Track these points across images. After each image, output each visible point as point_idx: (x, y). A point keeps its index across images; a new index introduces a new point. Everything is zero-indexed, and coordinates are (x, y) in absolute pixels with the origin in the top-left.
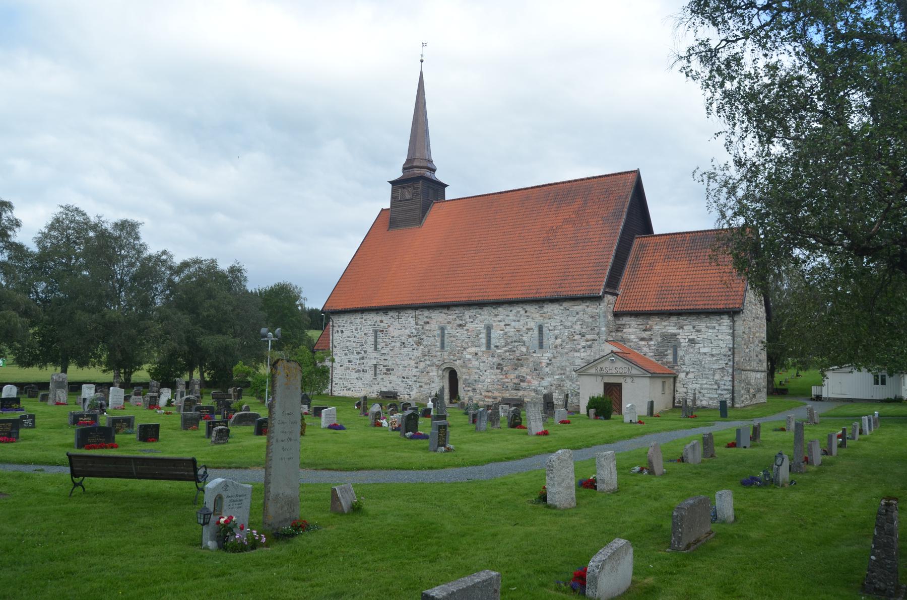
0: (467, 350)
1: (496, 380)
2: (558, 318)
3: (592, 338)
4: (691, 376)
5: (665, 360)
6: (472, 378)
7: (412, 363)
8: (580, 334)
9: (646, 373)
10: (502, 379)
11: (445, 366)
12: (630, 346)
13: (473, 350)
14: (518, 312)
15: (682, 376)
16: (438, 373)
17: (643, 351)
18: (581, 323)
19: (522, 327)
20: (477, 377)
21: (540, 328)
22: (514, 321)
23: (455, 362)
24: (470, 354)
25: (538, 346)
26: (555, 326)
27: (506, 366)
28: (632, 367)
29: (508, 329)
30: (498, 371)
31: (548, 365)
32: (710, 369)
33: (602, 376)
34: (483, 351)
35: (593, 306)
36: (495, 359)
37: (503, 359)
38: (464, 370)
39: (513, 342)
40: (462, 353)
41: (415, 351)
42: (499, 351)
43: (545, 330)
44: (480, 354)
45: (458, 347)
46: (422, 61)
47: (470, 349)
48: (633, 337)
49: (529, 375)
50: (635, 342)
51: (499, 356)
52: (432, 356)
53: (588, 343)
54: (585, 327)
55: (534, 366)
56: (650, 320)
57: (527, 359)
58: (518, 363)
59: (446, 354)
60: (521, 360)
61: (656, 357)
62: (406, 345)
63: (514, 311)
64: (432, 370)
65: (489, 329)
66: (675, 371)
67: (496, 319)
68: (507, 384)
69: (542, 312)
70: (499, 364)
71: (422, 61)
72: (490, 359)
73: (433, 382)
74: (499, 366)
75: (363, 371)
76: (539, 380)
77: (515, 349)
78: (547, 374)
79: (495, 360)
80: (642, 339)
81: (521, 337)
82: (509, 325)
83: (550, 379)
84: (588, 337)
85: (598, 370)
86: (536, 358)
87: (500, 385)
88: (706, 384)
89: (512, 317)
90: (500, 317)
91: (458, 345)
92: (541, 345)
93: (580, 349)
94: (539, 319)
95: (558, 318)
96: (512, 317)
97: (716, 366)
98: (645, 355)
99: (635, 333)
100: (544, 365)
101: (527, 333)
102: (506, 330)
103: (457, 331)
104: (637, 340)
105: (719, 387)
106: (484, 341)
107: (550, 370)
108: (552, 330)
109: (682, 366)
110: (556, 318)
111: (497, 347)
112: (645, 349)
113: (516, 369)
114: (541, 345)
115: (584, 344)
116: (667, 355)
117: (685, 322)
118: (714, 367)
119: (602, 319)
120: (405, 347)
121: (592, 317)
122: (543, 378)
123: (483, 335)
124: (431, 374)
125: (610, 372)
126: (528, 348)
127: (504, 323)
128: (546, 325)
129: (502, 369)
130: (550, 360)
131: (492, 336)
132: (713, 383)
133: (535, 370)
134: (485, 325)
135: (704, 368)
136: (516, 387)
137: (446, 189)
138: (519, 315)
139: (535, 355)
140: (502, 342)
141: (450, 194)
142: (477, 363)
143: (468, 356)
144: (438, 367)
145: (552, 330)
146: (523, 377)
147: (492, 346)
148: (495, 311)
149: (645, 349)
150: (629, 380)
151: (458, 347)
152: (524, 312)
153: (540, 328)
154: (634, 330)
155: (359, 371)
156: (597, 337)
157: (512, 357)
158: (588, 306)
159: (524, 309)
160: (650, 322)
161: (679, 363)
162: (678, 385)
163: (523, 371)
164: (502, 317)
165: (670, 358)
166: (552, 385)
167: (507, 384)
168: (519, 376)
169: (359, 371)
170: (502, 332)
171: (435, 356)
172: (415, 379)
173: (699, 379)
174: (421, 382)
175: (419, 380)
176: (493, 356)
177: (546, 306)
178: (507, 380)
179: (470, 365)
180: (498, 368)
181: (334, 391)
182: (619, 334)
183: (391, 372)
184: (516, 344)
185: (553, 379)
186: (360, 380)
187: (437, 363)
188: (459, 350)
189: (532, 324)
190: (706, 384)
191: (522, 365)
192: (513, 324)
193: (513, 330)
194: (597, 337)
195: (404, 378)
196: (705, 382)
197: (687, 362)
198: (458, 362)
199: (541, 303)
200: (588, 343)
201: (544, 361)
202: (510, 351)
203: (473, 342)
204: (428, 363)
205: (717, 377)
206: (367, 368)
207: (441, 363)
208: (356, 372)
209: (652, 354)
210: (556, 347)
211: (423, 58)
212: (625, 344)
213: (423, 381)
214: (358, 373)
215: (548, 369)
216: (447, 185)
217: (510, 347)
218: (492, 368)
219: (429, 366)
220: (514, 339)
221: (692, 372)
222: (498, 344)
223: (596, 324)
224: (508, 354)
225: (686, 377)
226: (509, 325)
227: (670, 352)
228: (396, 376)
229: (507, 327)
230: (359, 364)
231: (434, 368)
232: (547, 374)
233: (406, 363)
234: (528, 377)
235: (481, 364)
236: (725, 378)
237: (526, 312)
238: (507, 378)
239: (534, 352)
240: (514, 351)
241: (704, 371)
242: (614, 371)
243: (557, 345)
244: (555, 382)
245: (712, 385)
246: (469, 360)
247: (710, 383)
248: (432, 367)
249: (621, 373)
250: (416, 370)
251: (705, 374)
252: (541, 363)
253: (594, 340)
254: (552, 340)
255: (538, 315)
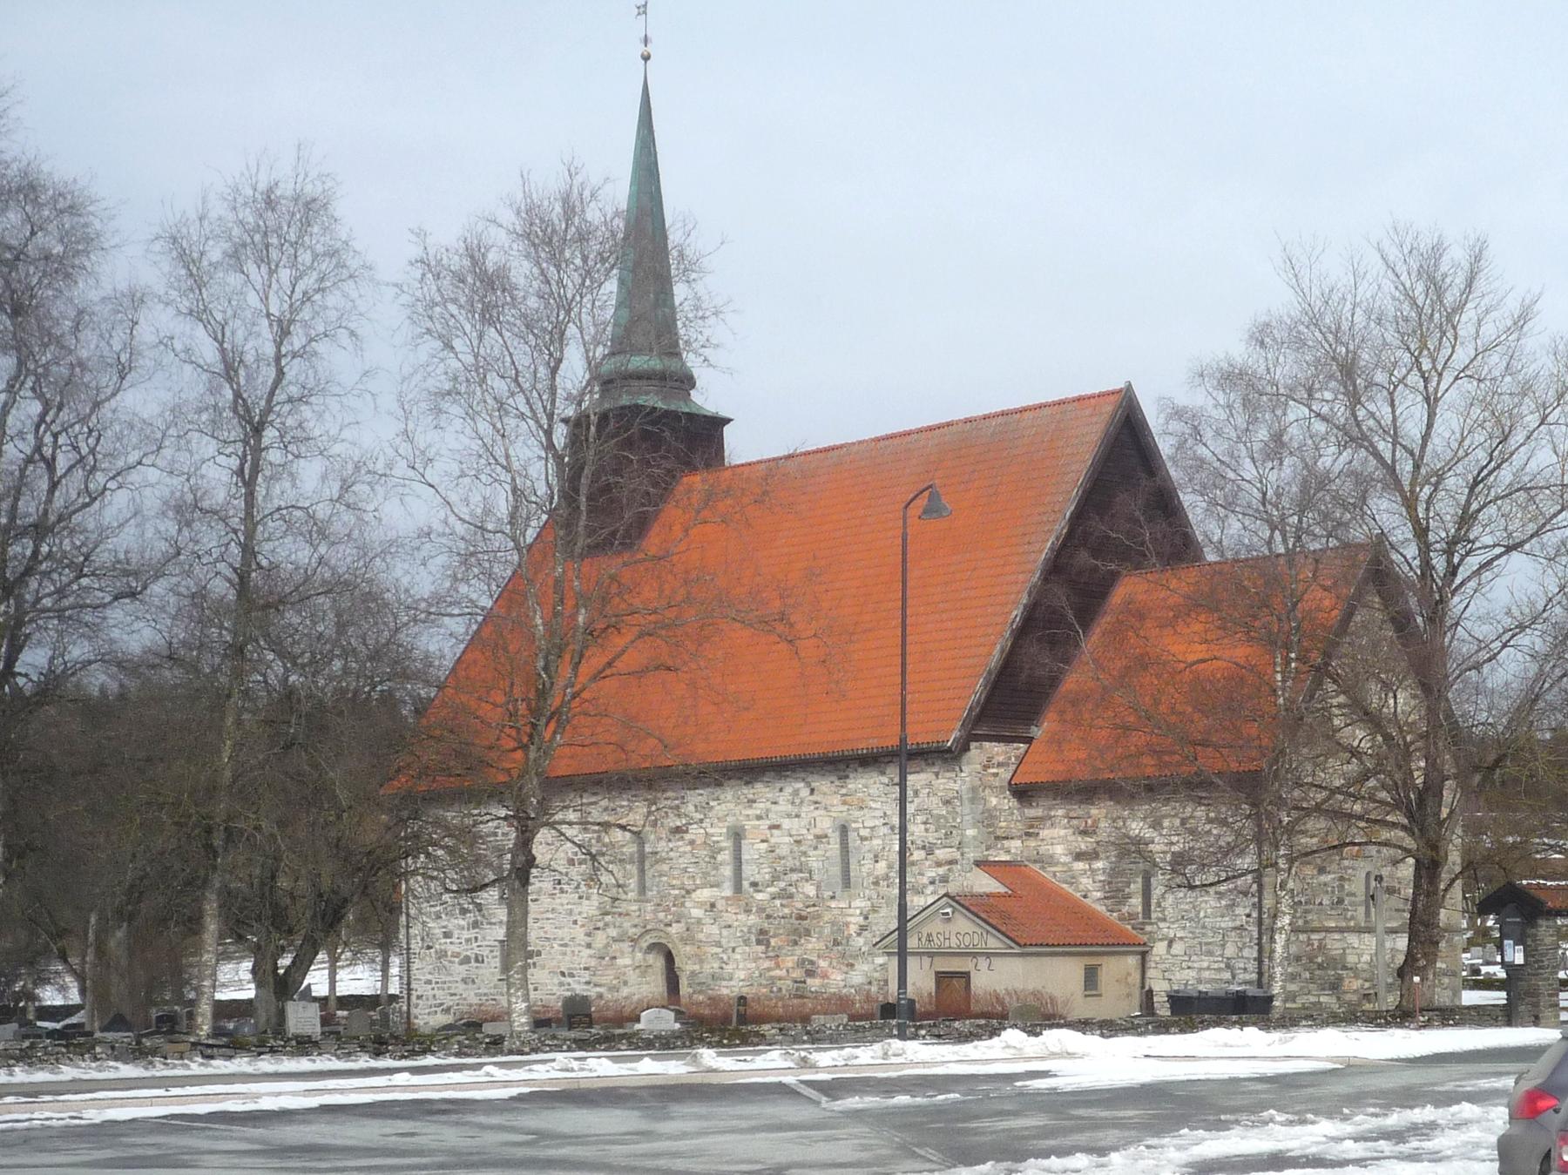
0: (693, 895)
1: (757, 974)
2: (878, 805)
3: (949, 857)
4: (1178, 948)
5: (1125, 909)
6: (707, 968)
7: (579, 933)
8: (924, 848)
9: (1013, 945)
10: (769, 969)
11: (649, 940)
12: (1055, 876)
13: (705, 894)
14: (796, 792)
15: (1160, 948)
16: (633, 958)
17: (1081, 887)
18: (923, 818)
19: (805, 832)
20: (716, 965)
21: (844, 830)
22: (789, 816)
23: (669, 929)
24: (700, 904)
25: (839, 881)
26: (872, 828)
27: (774, 936)
28: (988, 932)
29: (777, 837)
30: (761, 948)
31: (863, 928)
32: (1215, 930)
33: (931, 955)
34: (727, 899)
35: (948, 775)
36: (752, 917)
37: (768, 917)
38: (688, 948)
39: (788, 870)
40: (683, 904)
41: (585, 902)
42: (759, 896)
43: (852, 836)
44: (720, 905)
45: (673, 887)
46: (646, 58)
47: (698, 892)
48: (1059, 850)
49: (824, 958)
50: (1064, 864)
51: (761, 910)
52: (620, 914)
53: (941, 871)
54: (932, 828)
55: (832, 933)
56: (1093, 804)
57: (819, 916)
58: (801, 926)
59: (649, 907)
60: (806, 918)
61: (1108, 902)
62: (565, 887)
63: (788, 790)
64: (622, 953)
65: (737, 835)
66: (1145, 938)
67: (749, 812)
68: (779, 983)
69: (844, 791)
70: (762, 932)
71: (646, 58)
72: (742, 917)
73: (625, 983)
74: (762, 937)
75: (477, 960)
76: (845, 969)
77: (793, 890)
78: (860, 954)
79: (753, 919)
80: (1079, 856)
81: (803, 859)
82: (777, 827)
83: (866, 967)
84: (941, 854)
85: (923, 940)
86: (836, 912)
87: (766, 986)
88: (1208, 968)
89: (784, 806)
90: (759, 808)
91: (674, 882)
92: (847, 882)
93: (925, 887)
94: (839, 810)
95: (878, 805)
96: (784, 806)
97: (1227, 923)
98: (1085, 897)
99: (1064, 840)
100: (853, 929)
101: (816, 848)
102: (773, 840)
103: (671, 845)
104: (1068, 859)
105: (1234, 977)
106: (727, 871)
107: (865, 944)
108: (866, 839)
109: (1162, 925)
110: (874, 805)
111: (754, 884)
112: (1084, 880)
113: (796, 943)
114: (847, 882)
115: (931, 873)
116: (1129, 896)
117: (1165, 810)
118: (1223, 925)
119: (967, 808)
120: (562, 891)
121: (947, 802)
122: (852, 965)
123: (725, 856)
124: (619, 962)
125: (947, 944)
126: (818, 888)
127: (768, 822)
128: (853, 825)
129: (768, 945)
130: (866, 918)
131: (745, 857)
132: (1223, 965)
133: (836, 943)
134: (728, 828)
135: (1204, 927)
136: (797, 989)
137: (727, 429)
138: (797, 801)
139: (833, 904)
140: (764, 875)
141: (740, 446)
142: (715, 930)
143: (697, 913)
144: (634, 941)
145: (866, 839)
146: (812, 963)
147: (746, 884)
148: (748, 792)
149: (1086, 882)
150: (983, 963)
151: (673, 887)
152: (808, 791)
153: (844, 830)
154: (1062, 832)
155: (466, 960)
156: (957, 855)
157: (786, 911)
158: (937, 774)
159: (808, 784)
160: (1094, 811)
161: (1154, 916)
162: (1150, 973)
163: (810, 946)
164: (762, 805)
165: (1136, 903)
166: (870, 983)
167: (779, 983)
168: (804, 961)
169: (466, 960)
170: (765, 845)
171: (627, 914)
172: (586, 976)
173: (1194, 958)
174: (600, 986)
175: (595, 979)
176: (748, 911)
177: (851, 775)
178: (777, 973)
179: (701, 936)
180: (759, 942)
181: (416, 1017)
182: (1032, 843)
183: (535, 959)
184: (795, 876)
185: (872, 967)
186: (470, 986)
187: (632, 931)
188: (676, 897)
189: (825, 824)
190: (1208, 968)
191: (808, 933)
192: (786, 823)
193: (787, 839)
194: (957, 855)
195: (563, 974)
196: (1205, 965)
197: (1169, 912)
198: (675, 929)
199: (842, 766)
200: (941, 871)
201: (852, 919)
202: (785, 895)
203: (705, 874)
204: (613, 932)
205: (1230, 951)
206: (486, 952)
207: (638, 931)
208: (461, 963)
209: (1099, 894)
210: (876, 883)
211: (650, 48)
212: (1043, 868)
213: (603, 980)
214: (465, 967)
215: (861, 941)
216: (729, 421)
217: (782, 884)
218: (746, 942)
219: (615, 940)
220: (790, 863)
221: (1181, 938)
222: (758, 878)
223: (954, 820)
224: (778, 902)
225: (1168, 952)
226: (777, 827)
227: (1136, 886)
228: (547, 971)
229: (775, 832)
230: (468, 940)
231: (626, 946)
232: (860, 954)
233: (564, 933)
234: (823, 964)
235: (725, 932)
236: (1246, 953)
237: (812, 791)
238: (778, 966)
239: (833, 898)
240: (791, 896)
241: (1204, 935)
242: (954, 942)
243: (877, 877)
244: (876, 975)
245: (1219, 970)
246: (699, 921)
247: (1216, 966)
248: (621, 944)
249: (967, 947)
250: (589, 951)
251: (1206, 944)
252: (847, 924)
253: (952, 862)
254: (868, 864)
255: (836, 800)
